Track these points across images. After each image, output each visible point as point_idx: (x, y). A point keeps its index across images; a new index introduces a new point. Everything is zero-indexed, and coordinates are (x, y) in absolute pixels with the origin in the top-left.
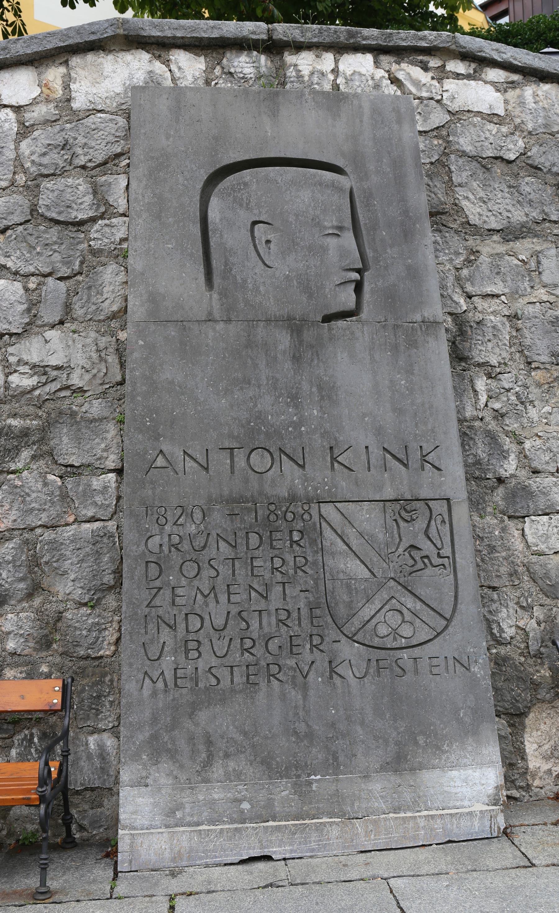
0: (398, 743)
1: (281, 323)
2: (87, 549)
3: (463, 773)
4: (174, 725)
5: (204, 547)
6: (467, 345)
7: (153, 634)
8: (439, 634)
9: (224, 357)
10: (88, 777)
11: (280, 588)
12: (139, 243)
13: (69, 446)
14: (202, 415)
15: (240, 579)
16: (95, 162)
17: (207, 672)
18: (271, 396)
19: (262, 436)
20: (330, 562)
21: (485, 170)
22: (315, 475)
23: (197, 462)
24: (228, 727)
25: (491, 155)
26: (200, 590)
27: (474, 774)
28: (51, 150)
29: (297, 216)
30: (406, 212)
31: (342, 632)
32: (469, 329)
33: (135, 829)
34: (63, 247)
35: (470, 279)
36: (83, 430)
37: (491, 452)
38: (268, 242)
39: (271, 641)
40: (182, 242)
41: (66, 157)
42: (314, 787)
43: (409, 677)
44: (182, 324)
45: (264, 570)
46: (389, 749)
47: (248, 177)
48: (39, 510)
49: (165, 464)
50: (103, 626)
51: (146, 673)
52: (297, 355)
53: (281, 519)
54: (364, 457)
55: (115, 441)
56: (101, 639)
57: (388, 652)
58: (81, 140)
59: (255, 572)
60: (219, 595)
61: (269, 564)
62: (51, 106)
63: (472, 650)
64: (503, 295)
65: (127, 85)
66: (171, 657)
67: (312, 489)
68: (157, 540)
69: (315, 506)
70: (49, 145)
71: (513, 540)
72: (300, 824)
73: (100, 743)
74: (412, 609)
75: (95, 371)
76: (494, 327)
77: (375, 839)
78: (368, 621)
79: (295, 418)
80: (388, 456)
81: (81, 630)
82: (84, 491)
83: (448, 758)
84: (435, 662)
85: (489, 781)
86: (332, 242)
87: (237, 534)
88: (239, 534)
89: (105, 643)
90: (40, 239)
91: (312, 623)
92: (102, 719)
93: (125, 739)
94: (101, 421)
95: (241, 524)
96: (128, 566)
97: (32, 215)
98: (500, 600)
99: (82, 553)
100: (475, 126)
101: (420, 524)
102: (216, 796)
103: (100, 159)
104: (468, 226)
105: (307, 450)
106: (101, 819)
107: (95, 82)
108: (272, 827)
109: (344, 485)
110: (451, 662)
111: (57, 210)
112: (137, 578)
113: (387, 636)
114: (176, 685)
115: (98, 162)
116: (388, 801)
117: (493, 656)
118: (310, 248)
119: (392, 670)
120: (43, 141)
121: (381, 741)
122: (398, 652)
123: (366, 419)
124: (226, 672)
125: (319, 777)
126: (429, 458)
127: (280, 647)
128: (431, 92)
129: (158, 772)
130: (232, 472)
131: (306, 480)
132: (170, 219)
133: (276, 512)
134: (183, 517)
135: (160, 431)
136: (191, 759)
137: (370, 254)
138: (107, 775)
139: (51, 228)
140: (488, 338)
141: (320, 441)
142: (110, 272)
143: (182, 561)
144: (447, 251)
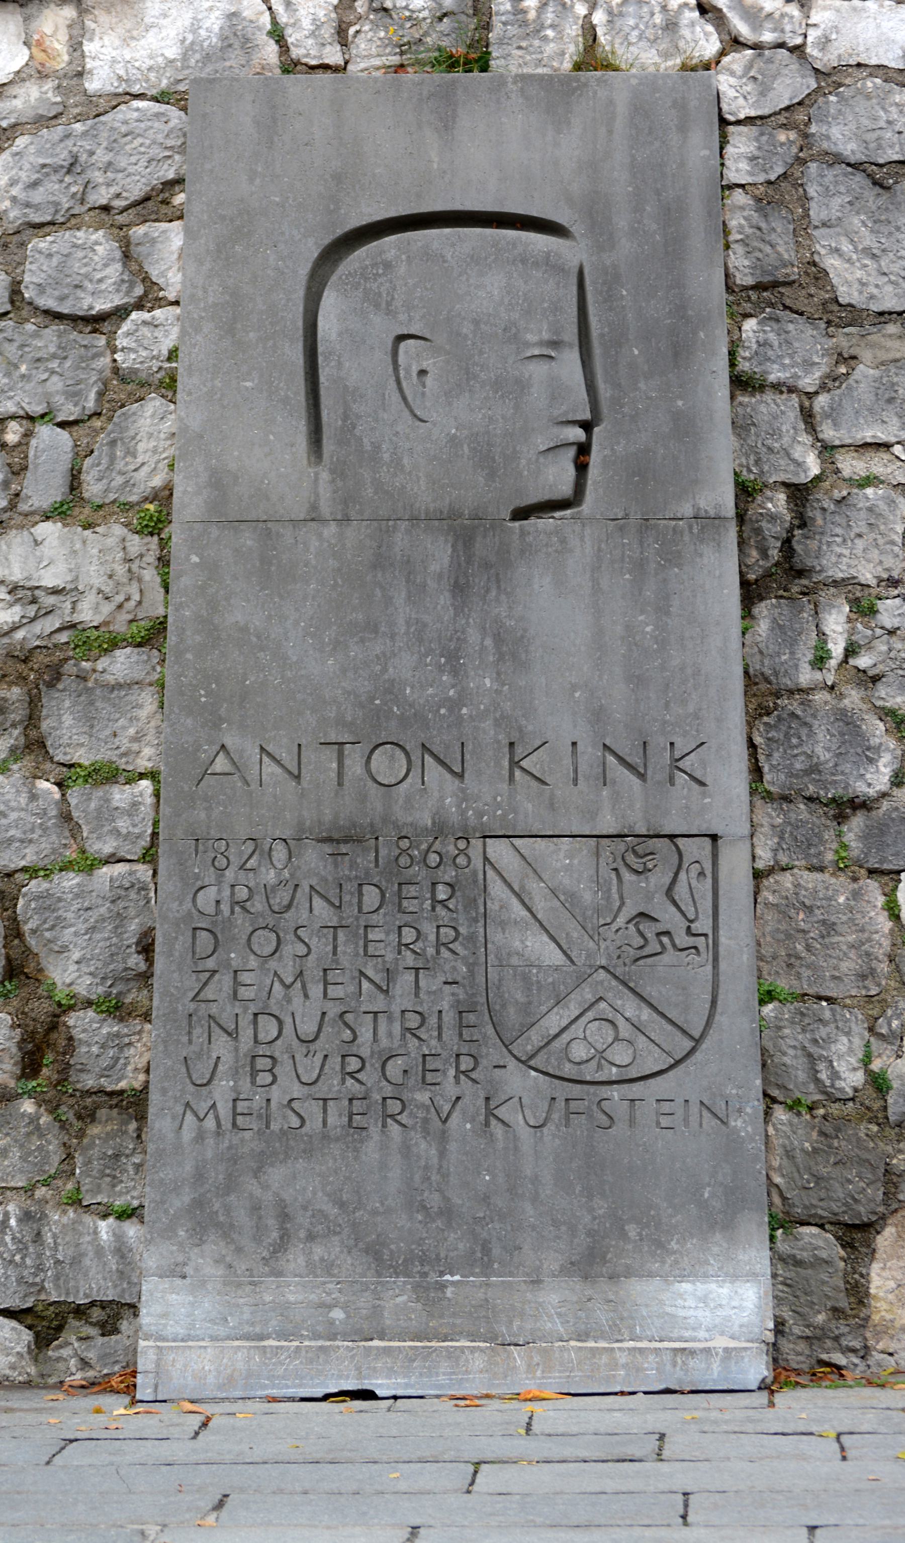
0: (590, 1233)
1: (436, 523)
2: (103, 910)
3: (701, 1287)
4: (230, 1185)
5: (289, 907)
6: (813, 544)
7: (202, 1044)
8: (678, 1063)
9: (335, 586)
10: (97, 1284)
11: (410, 977)
12: (195, 380)
13: (74, 731)
14: (292, 685)
15: (345, 961)
16: (126, 199)
17: (284, 1106)
18: (413, 654)
19: (393, 723)
20: (497, 937)
21: (881, 191)
22: (480, 791)
23: (282, 766)
24: (314, 1193)
25: (896, 157)
26: (279, 977)
27: (720, 1290)
28: (47, 174)
29: (476, 322)
30: (680, 310)
31: (510, 1052)
32: (818, 515)
33: (165, 1339)
34: (68, 363)
35: (833, 414)
36: (99, 704)
37: (842, 750)
38: (423, 373)
39: (390, 1062)
40: (270, 376)
41: (74, 189)
42: (449, 1292)
43: (620, 1129)
44: (265, 527)
45: (386, 946)
46: (576, 1241)
47: (393, 251)
48: (22, 841)
49: (228, 768)
50: (127, 1040)
51: (187, 1105)
52: (462, 581)
53: (418, 863)
54: (567, 761)
55: (153, 724)
56: (122, 1061)
57: (586, 1087)
58: (102, 156)
59: (371, 950)
60: (309, 986)
61: (394, 937)
62: (49, 85)
63: (734, 1091)
64: (898, 443)
65: (188, 42)
66: (228, 1081)
67: (474, 814)
68: (211, 893)
69: (477, 843)
70: (44, 166)
71: (873, 914)
72: (423, 1348)
73: (117, 1231)
74: (635, 1020)
75: (120, 598)
76: (870, 510)
77: (543, 1378)
78: (557, 1036)
79: (451, 693)
80: (611, 759)
81: (89, 1045)
82: (99, 810)
83: (676, 1262)
84: (666, 1107)
85: (745, 1304)
86: (538, 370)
87: (344, 887)
88: (347, 887)
89: (129, 1068)
90: (27, 349)
91: (461, 1035)
92: (121, 1194)
93: (153, 1205)
94: (130, 688)
95: (351, 871)
96: (164, 936)
97: (12, 302)
98: (836, 1021)
99: (93, 916)
100: (868, 97)
101: (660, 878)
102: (292, 1298)
103: (136, 192)
104: (836, 308)
105: (469, 747)
106: (116, 1351)
107: (128, 39)
108: (377, 1348)
109: (529, 811)
110: (695, 1108)
111: (57, 293)
112: (177, 954)
113: (587, 1061)
114: (234, 1124)
115: (132, 199)
116: (568, 1322)
117: (816, 1120)
118: (497, 384)
119: (591, 1117)
120: (31, 159)
121: (563, 1228)
122: (604, 1088)
123: (577, 695)
124: (315, 1108)
125: (457, 1278)
126: (685, 764)
127: (405, 1071)
128: (783, 31)
129: (202, 1257)
130: (340, 784)
131: (465, 799)
132: (251, 335)
133: (409, 852)
134: (255, 857)
135: (223, 712)
136: (255, 1239)
137: (604, 391)
138: (129, 1283)
139: (46, 327)
140: (857, 530)
141: (492, 732)
142: (149, 414)
143: (251, 929)
144: (787, 361)
